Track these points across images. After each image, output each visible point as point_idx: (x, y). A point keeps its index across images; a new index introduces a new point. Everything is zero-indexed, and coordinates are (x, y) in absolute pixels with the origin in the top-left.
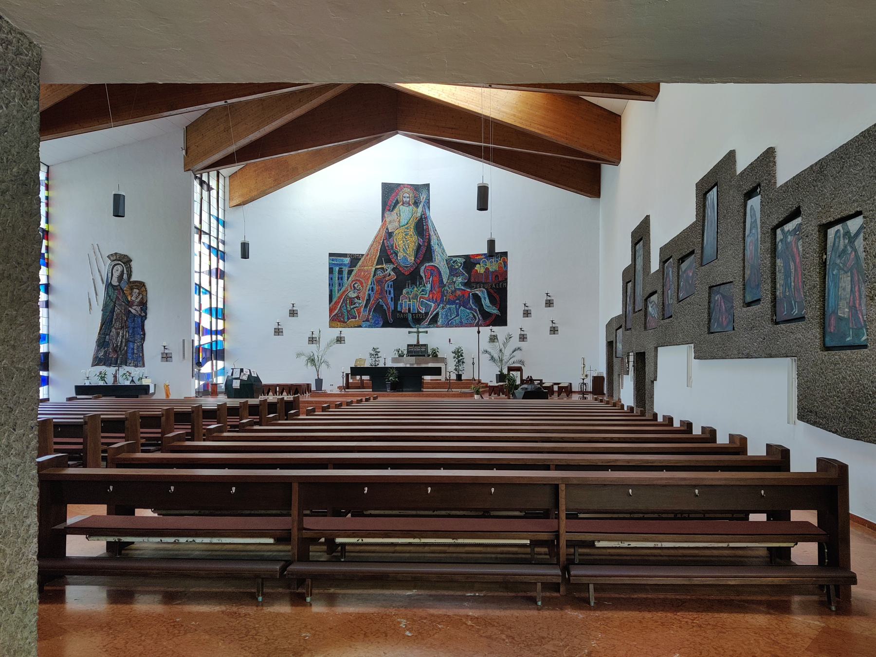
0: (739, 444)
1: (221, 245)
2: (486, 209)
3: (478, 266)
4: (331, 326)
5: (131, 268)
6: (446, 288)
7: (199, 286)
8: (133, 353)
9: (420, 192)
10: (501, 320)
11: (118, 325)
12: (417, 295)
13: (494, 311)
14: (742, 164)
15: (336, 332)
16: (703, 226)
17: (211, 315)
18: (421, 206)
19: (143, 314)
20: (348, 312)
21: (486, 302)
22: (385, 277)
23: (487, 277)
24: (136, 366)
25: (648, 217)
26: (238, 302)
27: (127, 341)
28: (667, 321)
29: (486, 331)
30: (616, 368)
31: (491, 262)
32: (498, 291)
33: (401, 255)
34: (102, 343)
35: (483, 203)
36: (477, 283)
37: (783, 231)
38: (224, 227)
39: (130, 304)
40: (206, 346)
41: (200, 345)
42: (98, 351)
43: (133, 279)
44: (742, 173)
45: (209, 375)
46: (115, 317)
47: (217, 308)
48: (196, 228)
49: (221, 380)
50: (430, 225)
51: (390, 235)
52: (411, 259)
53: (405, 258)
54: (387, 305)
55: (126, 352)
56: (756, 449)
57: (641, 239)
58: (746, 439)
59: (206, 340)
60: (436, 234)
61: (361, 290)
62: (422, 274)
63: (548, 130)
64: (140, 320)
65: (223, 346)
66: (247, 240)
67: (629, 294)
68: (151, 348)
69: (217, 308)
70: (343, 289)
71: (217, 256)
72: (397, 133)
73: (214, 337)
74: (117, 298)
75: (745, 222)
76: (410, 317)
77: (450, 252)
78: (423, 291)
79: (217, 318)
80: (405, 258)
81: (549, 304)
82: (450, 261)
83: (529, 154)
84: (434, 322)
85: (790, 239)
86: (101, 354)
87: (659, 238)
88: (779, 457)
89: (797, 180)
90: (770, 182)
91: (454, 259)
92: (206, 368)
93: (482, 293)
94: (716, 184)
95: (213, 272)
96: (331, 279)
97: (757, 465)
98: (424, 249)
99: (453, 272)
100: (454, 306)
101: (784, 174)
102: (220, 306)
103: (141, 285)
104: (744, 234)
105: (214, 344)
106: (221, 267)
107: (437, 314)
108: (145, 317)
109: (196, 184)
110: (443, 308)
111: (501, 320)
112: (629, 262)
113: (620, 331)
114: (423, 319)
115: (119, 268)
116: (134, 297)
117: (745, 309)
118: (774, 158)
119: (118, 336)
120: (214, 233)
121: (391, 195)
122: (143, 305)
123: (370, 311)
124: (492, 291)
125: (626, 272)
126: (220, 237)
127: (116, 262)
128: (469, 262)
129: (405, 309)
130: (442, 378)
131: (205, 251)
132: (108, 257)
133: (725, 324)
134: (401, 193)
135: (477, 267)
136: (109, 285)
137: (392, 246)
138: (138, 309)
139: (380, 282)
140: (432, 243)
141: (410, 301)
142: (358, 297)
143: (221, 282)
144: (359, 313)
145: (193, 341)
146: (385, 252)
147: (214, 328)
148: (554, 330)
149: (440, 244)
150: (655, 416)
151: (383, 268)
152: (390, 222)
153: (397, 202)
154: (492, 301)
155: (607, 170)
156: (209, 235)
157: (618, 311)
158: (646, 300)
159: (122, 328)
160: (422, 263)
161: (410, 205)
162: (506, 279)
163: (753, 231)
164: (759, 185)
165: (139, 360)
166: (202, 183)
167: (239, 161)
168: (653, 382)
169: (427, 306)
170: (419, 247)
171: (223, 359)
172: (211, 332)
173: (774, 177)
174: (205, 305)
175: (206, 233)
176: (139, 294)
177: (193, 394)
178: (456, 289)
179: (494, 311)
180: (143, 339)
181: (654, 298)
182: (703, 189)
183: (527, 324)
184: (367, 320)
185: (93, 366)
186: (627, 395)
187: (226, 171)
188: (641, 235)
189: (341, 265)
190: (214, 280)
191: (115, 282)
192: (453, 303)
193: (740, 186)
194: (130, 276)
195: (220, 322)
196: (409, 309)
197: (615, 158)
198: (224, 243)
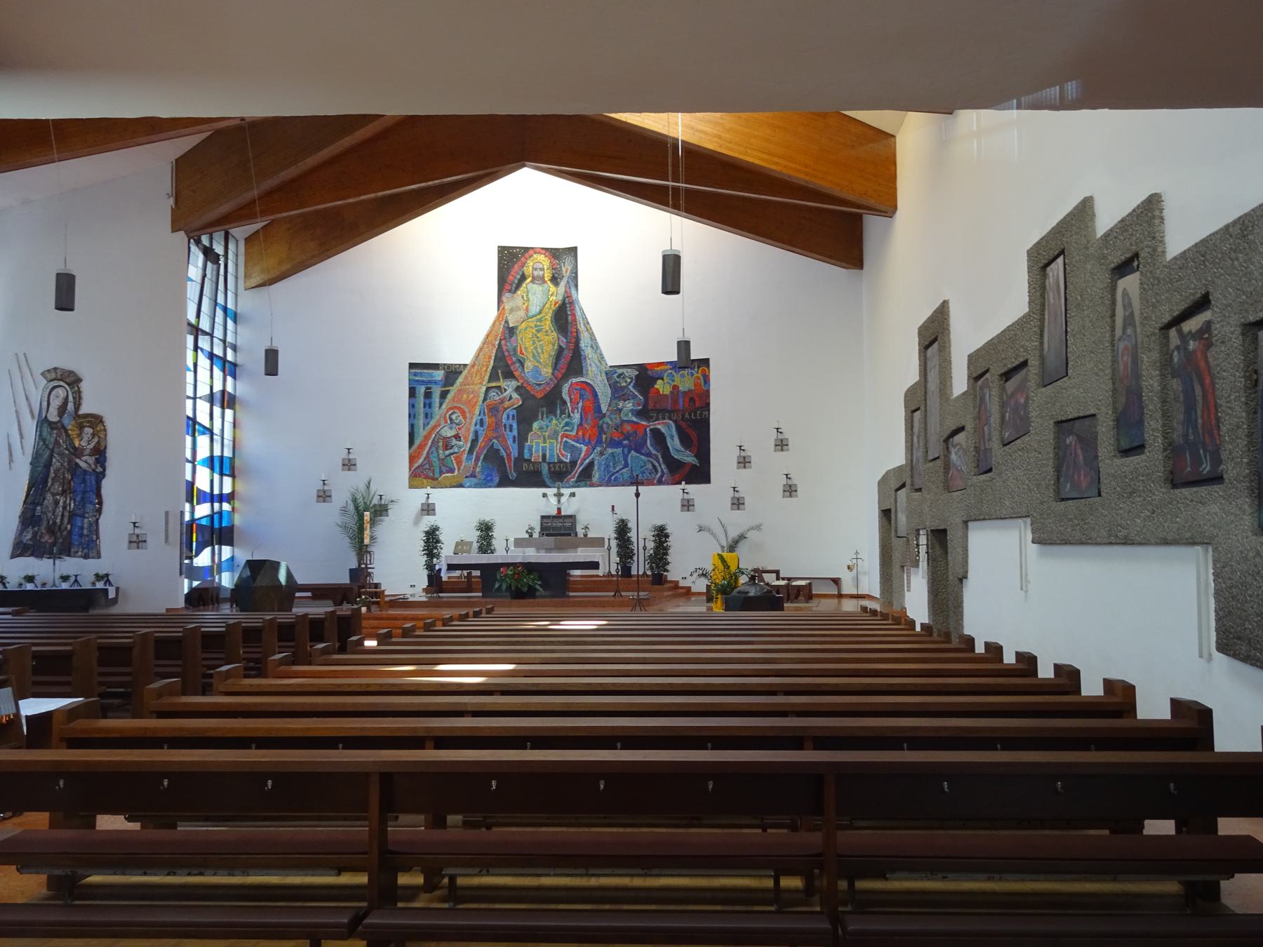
0: (1121, 696)
1: (230, 353)
2: (678, 292)
3: (659, 382)
4: (411, 487)
5: (79, 392)
6: (607, 419)
7: (193, 421)
8: (81, 535)
9: (563, 259)
10: (700, 474)
11: (58, 488)
12: (556, 433)
13: (689, 458)
14: (1105, 221)
15: (418, 496)
16: (1042, 320)
17: (212, 469)
18: (563, 284)
19: (99, 469)
20: (441, 461)
21: (674, 443)
22: (502, 401)
23: (675, 402)
24: (86, 557)
25: (945, 304)
26: (255, 443)
27: (72, 515)
28: (984, 477)
29: (673, 493)
30: (897, 556)
31: (683, 376)
32: (696, 429)
33: (529, 365)
34: (29, 518)
35: (671, 284)
36: (659, 411)
37: (1180, 332)
38: (235, 322)
39: (78, 452)
40: (204, 522)
41: (193, 520)
42: (21, 532)
43: (84, 410)
44: (1107, 235)
45: (209, 570)
46: (52, 475)
47: (222, 457)
48: (190, 324)
49: (227, 580)
50: (578, 314)
51: (511, 331)
52: (547, 371)
53: (536, 370)
54: (506, 448)
55: (70, 533)
56: (1153, 707)
57: (935, 340)
58: (1132, 688)
59: (203, 510)
60: (589, 330)
61: (462, 421)
62: (565, 396)
63: (776, 159)
64: (93, 478)
65: (231, 519)
66: (275, 345)
67: (916, 430)
68: (112, 525)
69: (222, 457)
70: (433, 423)
71: (223, 370)
72: (524, 166)
73: (216, 505)
74: (57, 443)
75: (1113, 315)
76: (545, 469)
77: (612, 360)
78: (567, 424)
79: (222, 474)
80: (536, 370)
81: (782, 445)
82: (613, 374)
83: (744, 198)
84: (586, 477)
85: (1192, 345)
86: (28, 536)
87: (967, 338)
88: (1193, 721)
89: (1202, 249)
90: (1155, 250)
91: (620, 371)
92: (203, 559)
93: (667, 428)
94: (1062, 252)
95: (218, 397)
96: (412, 406)
97: (1153, 736)
98: (568, 354)
99: (618, 392)
100: (619, 450)
101: (1180, 236)
102: (228, 453)
103: (96, 421)
104: (1113, 336)
105: (216, 517)
106: (229, 389)
107: (591, 464)
108: (103, 474)
109: (198, 257)
110: (601, 454)
111: (700, 474)
112: (913, 377)
113: (902, 493)
114: (567, 473)
115: (61, 393)
116: (85, 441)
117: (1118, 461)
118: (1161, 210)
119: (56, 505)
120: (218, 333)
121: (511, 264)
122: (100, 453)
123: (477, 459)
124: (684, 425)
125: (910, 394)
126: (230, 339)
127: (56, 383)
128: (645, 375)
129: (536, 456)
130: (600, 572)
131: (204, 362)
132: (43, 374)
133: (1084, 485)
134: (530, 263)
135: (659, 385)
136: (43, 422)
137: (515, 350)
138: (91, 460)
139: (494, 410)
140: (582, 345)
141: (546, 440)
142: (457, 437)
143: (229, 413)
144: (459, 463)
145: (182, 513)
146: (503, 358)
147: (216, 492)
148: (790, 490)
149: (595, 346)
150: (970, 641)
151: (499, 388)
152: (512, 310)
153: (523, 278)
154: (685, 440)
155: (872, 223)
156: (211, 335)
157: (898, 457)
158: (946, 440)
159: (64, 493)
160: (565, 377)
161: (544, 282)
162: (708, 404)
163: (1129, 331)
164: (1136, 255)
165: (90, 548)
166: (209, 253)
167: (264, 213)
168: (961, 580)
169: (573, 449)
170: (560, 351)
171: (231, 543)
172: (212, 498)
173: (1162, 242)
174: (203, 452)
175: (205, 333)
176: (93, 435)
177: (181, 603)
178: (623, 422)
179: (689, 458)
180: (99, 511)
181: (960, 438)
182: (1044, 257)
183: (743, 479)
184: (473, 475)
185: (13, 557)
186: (916, 603)
187: (240, 232)
188: (934, 335)
189: (430, 382)
190: (217, 410)
191: (53, 416)
192: (617, 444)
193: (1105, 257)
194: (77, 406)
195: (227, 481)
196: (544, 456)
197: (888, 208)
198: (234, 348)
